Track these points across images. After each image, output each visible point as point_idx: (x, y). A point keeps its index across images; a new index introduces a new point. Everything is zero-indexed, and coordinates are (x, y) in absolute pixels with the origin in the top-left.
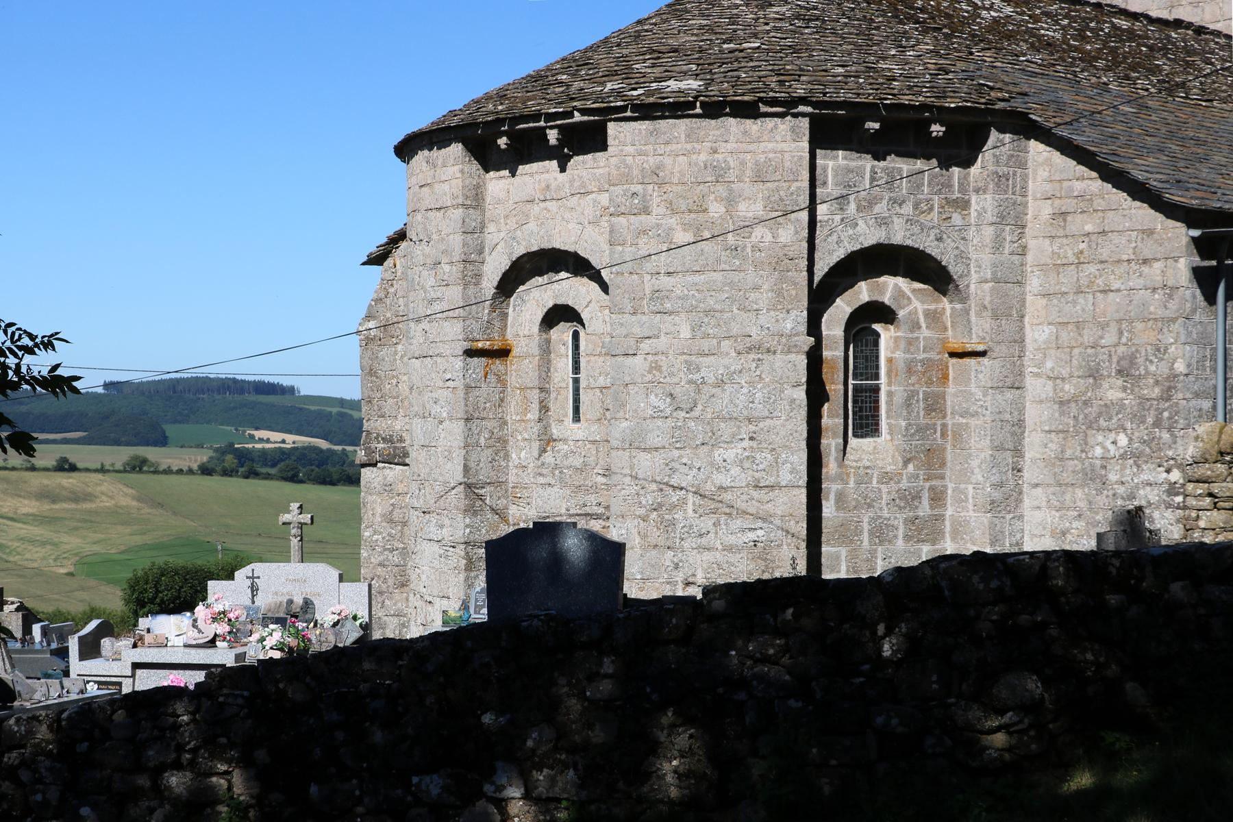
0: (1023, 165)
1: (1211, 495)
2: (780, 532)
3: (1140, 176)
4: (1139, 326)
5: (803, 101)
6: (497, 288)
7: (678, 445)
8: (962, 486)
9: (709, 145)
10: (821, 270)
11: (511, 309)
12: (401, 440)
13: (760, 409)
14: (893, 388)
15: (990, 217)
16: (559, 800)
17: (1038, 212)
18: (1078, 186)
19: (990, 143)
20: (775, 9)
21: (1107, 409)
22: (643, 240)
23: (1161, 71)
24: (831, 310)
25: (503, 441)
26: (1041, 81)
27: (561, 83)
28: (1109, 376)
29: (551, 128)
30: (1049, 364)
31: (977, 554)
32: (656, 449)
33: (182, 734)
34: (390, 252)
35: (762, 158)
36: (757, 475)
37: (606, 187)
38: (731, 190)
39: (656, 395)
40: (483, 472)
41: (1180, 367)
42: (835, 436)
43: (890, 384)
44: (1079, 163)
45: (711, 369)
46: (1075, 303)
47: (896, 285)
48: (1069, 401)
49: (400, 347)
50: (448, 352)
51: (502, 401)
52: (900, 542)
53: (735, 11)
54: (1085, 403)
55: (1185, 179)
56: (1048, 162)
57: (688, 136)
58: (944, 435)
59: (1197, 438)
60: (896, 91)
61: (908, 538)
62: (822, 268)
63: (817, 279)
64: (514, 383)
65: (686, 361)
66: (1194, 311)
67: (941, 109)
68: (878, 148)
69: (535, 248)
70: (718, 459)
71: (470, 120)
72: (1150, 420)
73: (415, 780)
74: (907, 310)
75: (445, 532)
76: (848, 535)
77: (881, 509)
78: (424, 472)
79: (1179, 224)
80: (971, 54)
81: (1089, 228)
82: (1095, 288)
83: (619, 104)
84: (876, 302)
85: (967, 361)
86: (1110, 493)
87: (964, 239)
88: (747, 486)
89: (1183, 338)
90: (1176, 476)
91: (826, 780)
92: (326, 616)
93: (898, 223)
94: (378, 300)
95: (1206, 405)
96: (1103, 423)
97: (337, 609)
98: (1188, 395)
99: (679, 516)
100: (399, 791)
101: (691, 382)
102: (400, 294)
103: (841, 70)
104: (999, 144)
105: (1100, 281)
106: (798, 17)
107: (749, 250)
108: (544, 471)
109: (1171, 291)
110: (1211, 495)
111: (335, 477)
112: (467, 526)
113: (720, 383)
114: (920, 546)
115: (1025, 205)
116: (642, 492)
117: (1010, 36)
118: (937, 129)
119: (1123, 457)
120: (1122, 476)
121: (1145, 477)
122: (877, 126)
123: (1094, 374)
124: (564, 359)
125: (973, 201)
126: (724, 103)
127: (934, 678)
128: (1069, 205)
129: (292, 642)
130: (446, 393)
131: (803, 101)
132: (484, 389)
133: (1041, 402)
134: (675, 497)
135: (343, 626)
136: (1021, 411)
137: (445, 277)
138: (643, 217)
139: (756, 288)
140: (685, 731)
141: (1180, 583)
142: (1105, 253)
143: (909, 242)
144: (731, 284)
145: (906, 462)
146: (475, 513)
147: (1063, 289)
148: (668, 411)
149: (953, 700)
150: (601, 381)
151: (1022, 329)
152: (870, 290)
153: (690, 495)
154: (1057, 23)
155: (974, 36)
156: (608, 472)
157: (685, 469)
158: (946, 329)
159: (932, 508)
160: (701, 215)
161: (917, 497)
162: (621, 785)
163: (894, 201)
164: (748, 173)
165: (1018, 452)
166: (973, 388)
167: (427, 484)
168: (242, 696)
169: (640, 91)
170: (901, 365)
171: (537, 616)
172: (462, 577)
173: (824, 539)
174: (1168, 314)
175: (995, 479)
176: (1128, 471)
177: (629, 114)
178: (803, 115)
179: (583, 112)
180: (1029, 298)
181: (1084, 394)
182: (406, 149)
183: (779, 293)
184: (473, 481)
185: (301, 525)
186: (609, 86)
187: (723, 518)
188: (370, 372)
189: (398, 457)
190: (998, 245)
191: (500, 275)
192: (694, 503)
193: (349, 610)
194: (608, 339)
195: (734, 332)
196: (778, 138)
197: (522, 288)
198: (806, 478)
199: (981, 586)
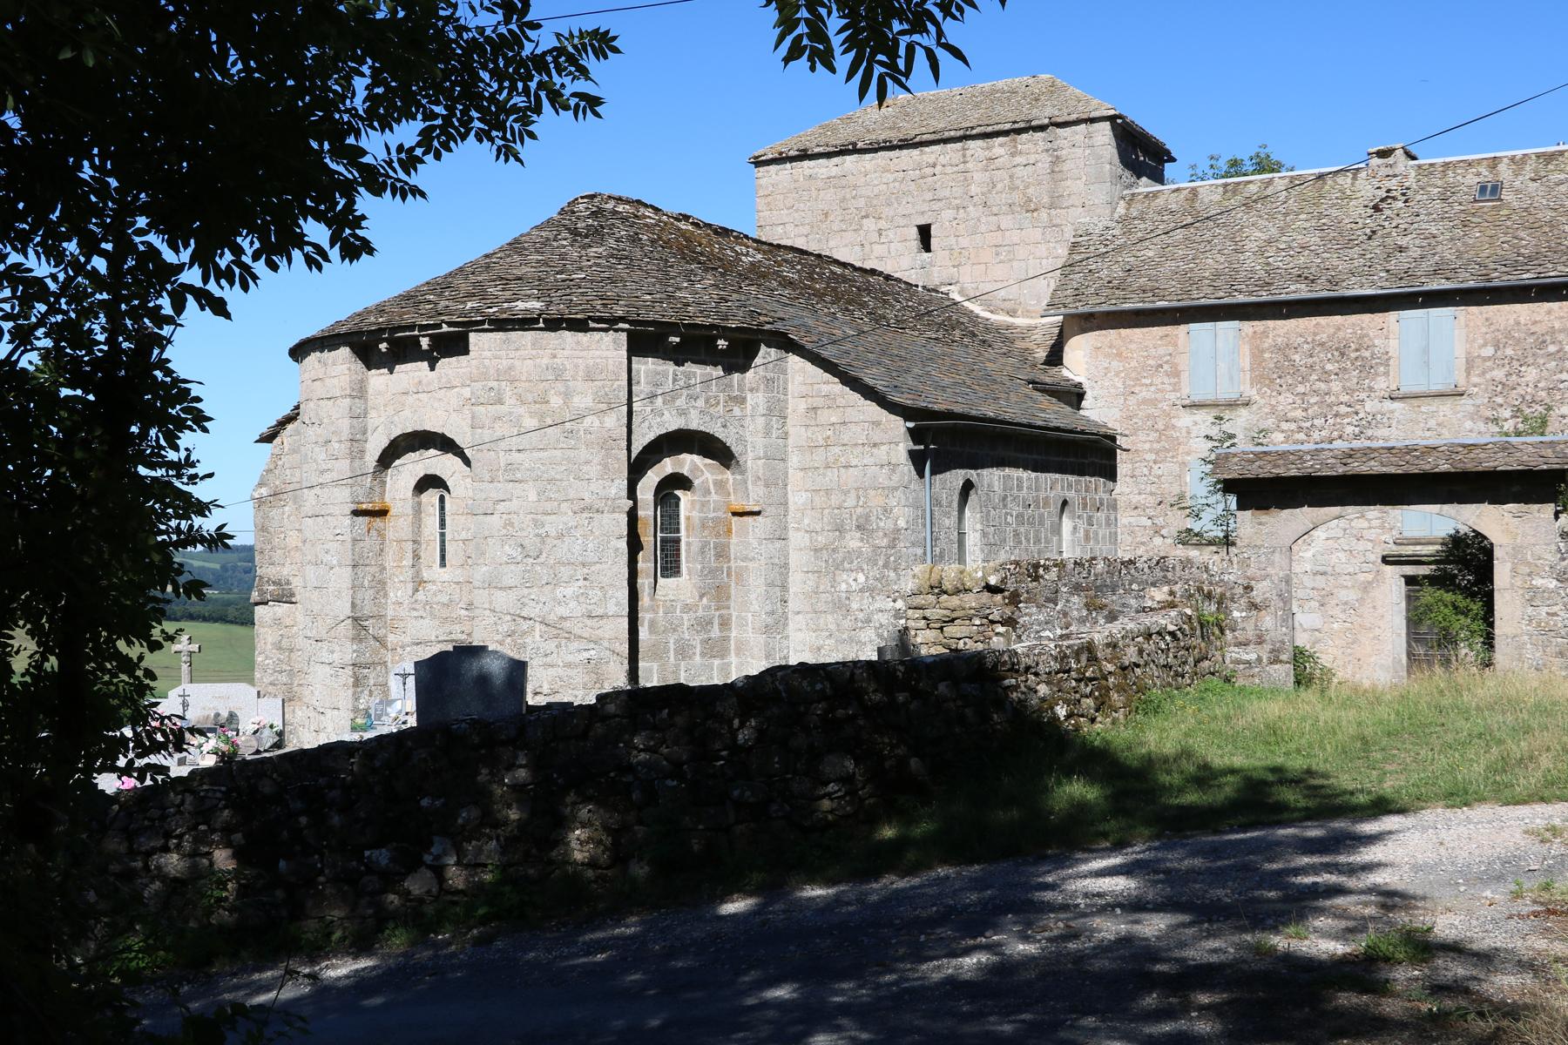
0: (784, 372)
1: (925, 618)
2: (608, 652)
3: (871, 382)
4: (872, 493)
5: (622, 319)
6: (378, 462)
7: (528, 585)
8: (743, 614)
9: (550, 351)
10: (637, 448)
11: (388, 478)
12: (288, 583)
13: (591, 557)
14: (691, 540)
15: (762, 410)
16: (485, 866)
17: (796, 406)
18: (825, 389)
19: (760, 354)
20: (594, 250)
21: (850, 555)
22: (498, 425)
23: (868, 306)
24: (644, 480)
25: (383, 583)
26: (791, 310)
27: (429, 302)
28: (851, 530)
29: (424, 336)
30: (806, 521)
31: (801, 664)
32: (510, 588)
33: (169, 824)
34: (279, 432)
35: (591, 362)
36: (590, 607)
37: (468, 382)
38: (567, 387)
39: (510, 546)
40: (367, 607)
41: (902, 523)
42: (648, 576)
43: (688, 537)
44: (825, 371)
45: (552, 525)
46: (824, 475)
47: (692, 460)
48: (821, 549)
49: (287, 509)
50: (338, 512)
51: (382, 551)
52: (698, 658)
53: (563, 250)
54: (833, 550)
55: (899, 385)
56: (803, 370)
57: (533, 344)
58: (729, 575)
59: (914, 576)
60: (691, 314)
61: (703, 655)
62: (637, 447)
63: (634, 456)
64: (392, 537)
65: (533, 519)
66: (910, 482)
67: (725, 328)
68: (678, 356)
69: (409, 430)
70: (560, 596)
71: (356, 329)
72: (881, 563)
73: (367, 853)
74: (701, 480)
75: (336, 656)
76: (659, 654)
77: (683, 632)
78: (316, 609)
79: (898, 418)
80: (741, 288)
81: (833, 419)
82: (839, 464)
83: (479, 318)
84: (678, 473)
85: (745, 518)
86: (853, 618)
87: (742, 426)
88: (582, 616)
89: (903, 503)
90: (900, 604)
91: (696, 841)
92: (247, 725)
93: (694, 414)
94: (269, 471)
95: (919, 551)
96: (846, 565)
97: (257, 720)
98: (908, 545)
99: (528, 640)
100: (354, 863)
101: (537, 535)
102: (286, 466)
103: (648, 297)
104: (766, 354)
105: (842, 459)
106: (612, 256)
107: (582, 433)
108: (417, 607)
109: (893, 467)
110: (925, 618)
111: (179, 614)
112: (354, 651)
113: (560, 536)
114: (712, 660)
115: (786, 401)
116: (499, 622)
117: (764, 276)
118: (722, 344)
119: (861, 591)
120: (862, 605)
121: (877, 605)
122: (678, 340)
123: (840, 529)
124: (432, 518)
125: (748, 399)
126: (561, 320)
127: (776, 760)
128: (818, 402)
129: (224, 747)
130: (336, 545)
131: (622, 319)
132: (367, 543)
133: (801, 549)
134: (525, 625)
135: (261, 733)
136: (786, 557)
137: (335, 453)
138: (498, 407)
139: (587, 462)
140: (585, 807)
141: (945, 683)
142: (845, 438)
143: (702, 428)
144: (568, 460)
145: (701, 596)
146: (361, 641)
147: (816, 465)
148: (519, 558)
149: (789, 776)
150: (464, 535)
151: (786, 494)
152: (673, 465)
153: (537, 624)
154: (793, 268)
155: (741, 275)
156: (470, 606)
157: (533, 604)
158: (729, 494)
159: (721, 631)
160: (544, 405)
161: (710, 623)
162: (534, 851)
163: (690, 397)
164: (581, 373)
165: (784, 587)
166: (751, 539)
167: (319, 618)
168: (220, 791)
169: (495, 309)
170: (697, 522)
171: (464, 720)
172: (350, 692)
173: (640, 656)
174: (892, 484)
175: (768, 608)
176: (865, 601)
177: (486, 326)
178: (623, 330)
179: (450, 324)
180: (791, 471)
181: (833, 543)
182: (299, 351)
183: (605, 466)
184: (359, 615)
185: (191, 653)
186: (469, 305)
187: (564, 641)
188: (262, 529)
189: (286, 597)
190: (767, 433)
191: (380, 451)
192: (540, 631)
193: (267, 721)
194: (471, 502)
195: (571, 497)
196: (603, 347)
197: (397, 462)
198: (627, 610)
199: (809, 689)
